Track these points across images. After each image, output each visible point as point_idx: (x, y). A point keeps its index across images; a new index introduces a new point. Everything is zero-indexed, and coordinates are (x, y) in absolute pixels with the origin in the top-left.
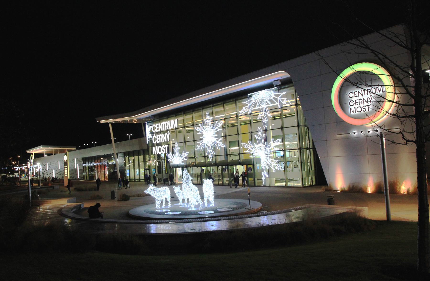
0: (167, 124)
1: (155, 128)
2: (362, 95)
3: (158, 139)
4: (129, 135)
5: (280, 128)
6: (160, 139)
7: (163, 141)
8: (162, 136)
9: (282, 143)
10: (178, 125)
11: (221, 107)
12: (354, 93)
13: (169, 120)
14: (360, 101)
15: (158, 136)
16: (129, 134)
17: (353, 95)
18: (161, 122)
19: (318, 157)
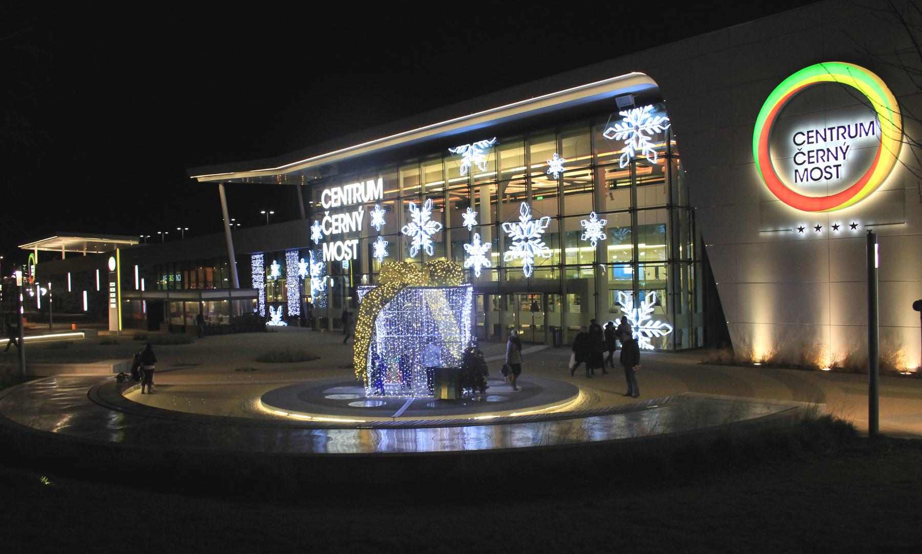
3: (334, 224)
6: (339, 224)
8: (346, 217)
14: (821, 154)
15: (334, 217)
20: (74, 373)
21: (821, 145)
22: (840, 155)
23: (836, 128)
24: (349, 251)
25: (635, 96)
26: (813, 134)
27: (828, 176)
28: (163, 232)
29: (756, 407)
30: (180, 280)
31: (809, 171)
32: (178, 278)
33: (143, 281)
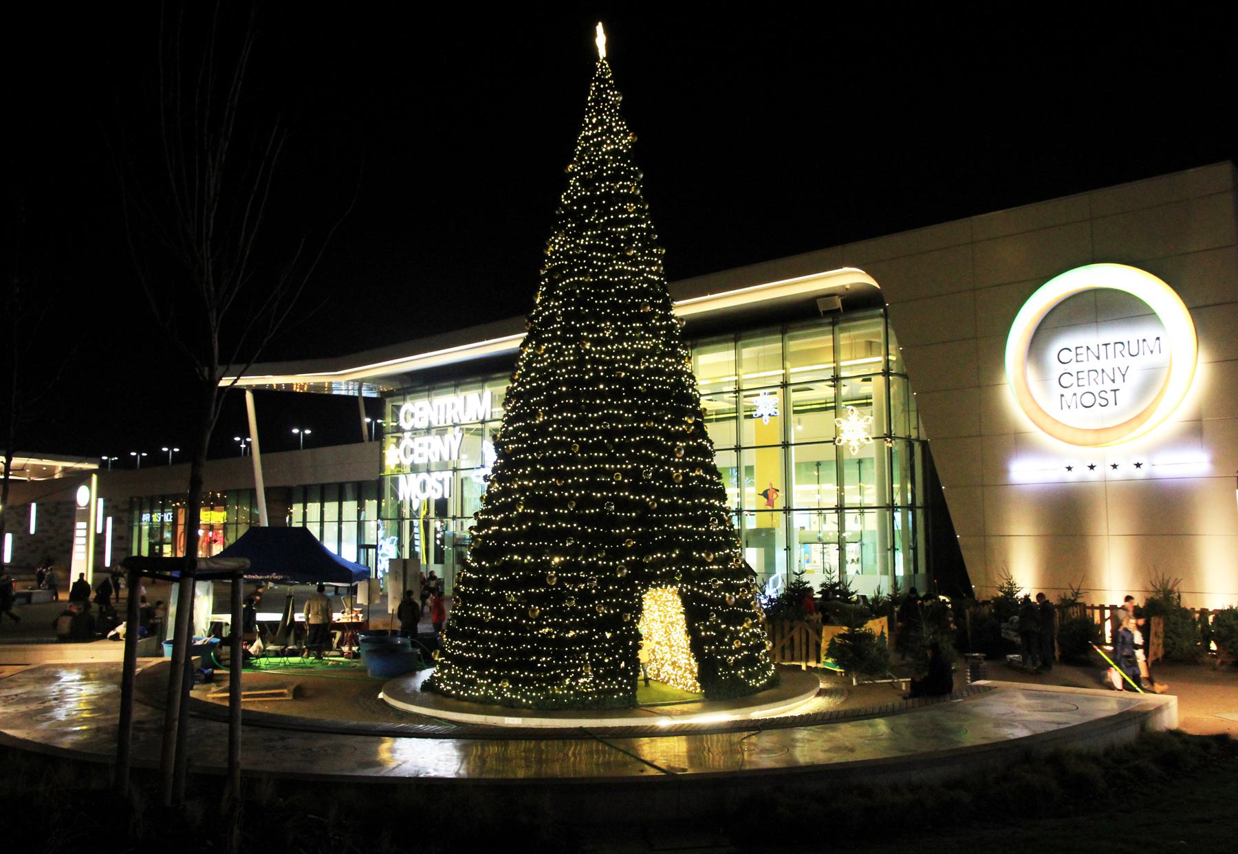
0: (453, 405)
1: (409, 417)
2: (1098, 358)
3: (417, 451)
4: (299, 433)
5: (781, 444)
6: (424, 450)
7: (438, 460)
8: (434, 439)
9: (817, 485)
10: (493, 410)
11: (823, 333)
12: (1073, 350)
13: (462, 391)
14: (1093, 374)
15: (418, 440)
16: (171, 448)
17: (1072, 355)
18: (433, 397)
19: (954, 532)
20: (62, 658)
21: (1094, 364)
22: (1119, 378)
23: (1112, 344)
24: (439, 486)
25: (843, 298)
26: (1083, 350)
27: (1104, 402)
28: (139, 452)
29: (992, 705)
30: (171, 520)
31: (1079, 395)
32: (168, 518)
33: (110, 520)
